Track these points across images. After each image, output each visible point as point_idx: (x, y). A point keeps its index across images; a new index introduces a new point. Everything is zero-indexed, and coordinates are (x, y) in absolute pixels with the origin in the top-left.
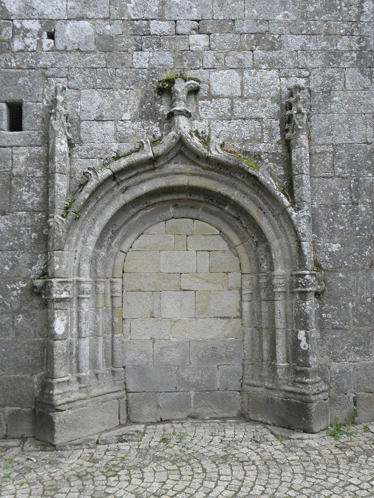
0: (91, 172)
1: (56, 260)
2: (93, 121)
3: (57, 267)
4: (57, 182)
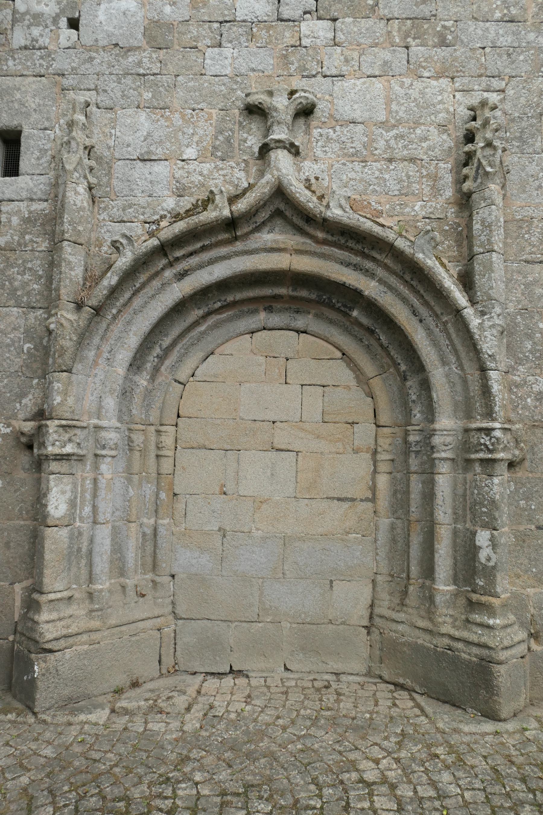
0: (124, 241)
1: (56, 388)
2: (134, 160)
3: (58, 399)
4: (66, 256)
